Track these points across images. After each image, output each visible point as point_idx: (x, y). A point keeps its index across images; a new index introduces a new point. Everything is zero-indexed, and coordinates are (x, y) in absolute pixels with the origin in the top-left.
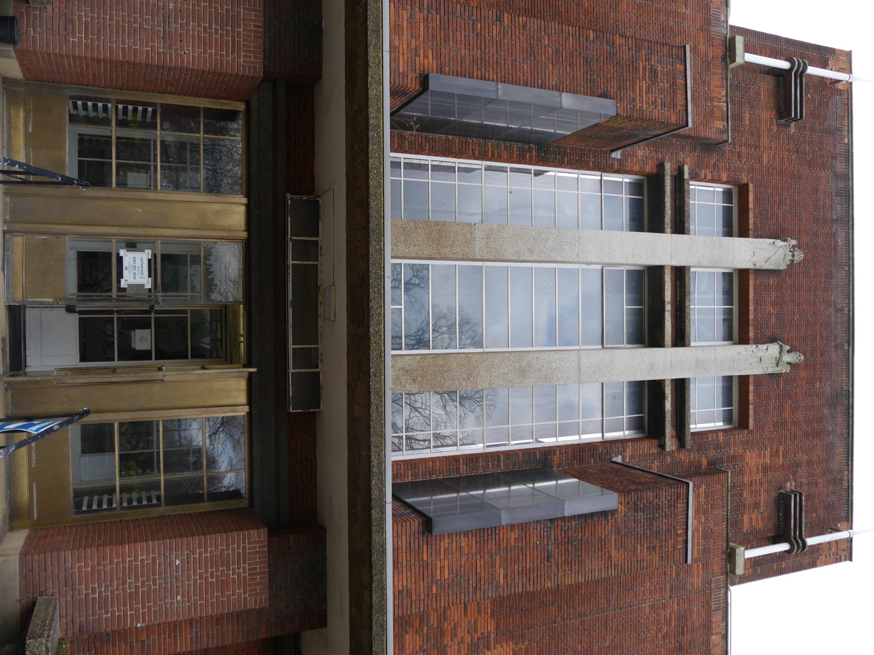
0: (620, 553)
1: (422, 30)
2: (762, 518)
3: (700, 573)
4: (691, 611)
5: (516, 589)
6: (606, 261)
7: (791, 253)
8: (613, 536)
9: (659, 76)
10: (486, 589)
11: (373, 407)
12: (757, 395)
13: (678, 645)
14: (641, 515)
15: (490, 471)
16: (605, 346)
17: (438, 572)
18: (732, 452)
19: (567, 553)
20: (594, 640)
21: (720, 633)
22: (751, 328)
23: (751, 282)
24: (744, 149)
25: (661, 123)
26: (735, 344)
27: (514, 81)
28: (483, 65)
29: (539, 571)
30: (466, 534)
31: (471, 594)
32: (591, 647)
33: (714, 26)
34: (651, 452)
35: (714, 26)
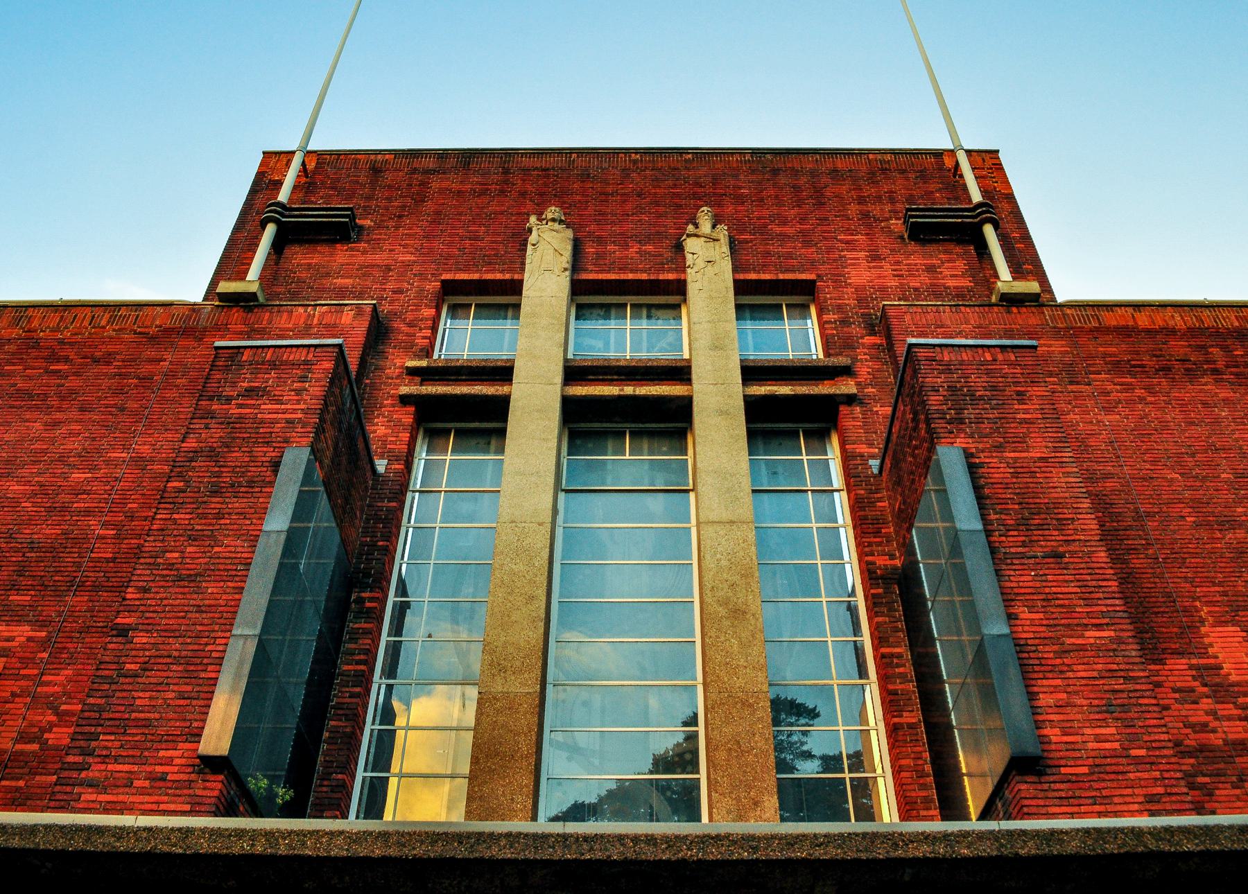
0: (1034, 444)
1: (121, 766)
2: (948, 261)
3: (1045, 342)
4: (1105, 355)
5: (1118, 608)
6: (551, 480)
7: (550, 223)
8: (1007, 454)
9: (257, 384)
10: (1125, 660)
11: (819, 853)
12: (764, 268)
13: (1161, 373)
14: (970, 413)
15: (909, 669)
16: (691, 487)
17: (1107, 745)
18: (853, 302)
19: (1045, 527)
20: (1177, 496)
21: (1132, 315)
22: (661, 277)
23: (591, 276)
24: (390, 285)
25: (332, 382)
26: (685, 301)
27: (232, 609)
28: (199, 661)
29: (1081, 571)
30: (1032, 696)
31: (1138, 687)
32: (1187, 501)
33: (197, 323)
34: (860, 416)
35: (197, 323)
